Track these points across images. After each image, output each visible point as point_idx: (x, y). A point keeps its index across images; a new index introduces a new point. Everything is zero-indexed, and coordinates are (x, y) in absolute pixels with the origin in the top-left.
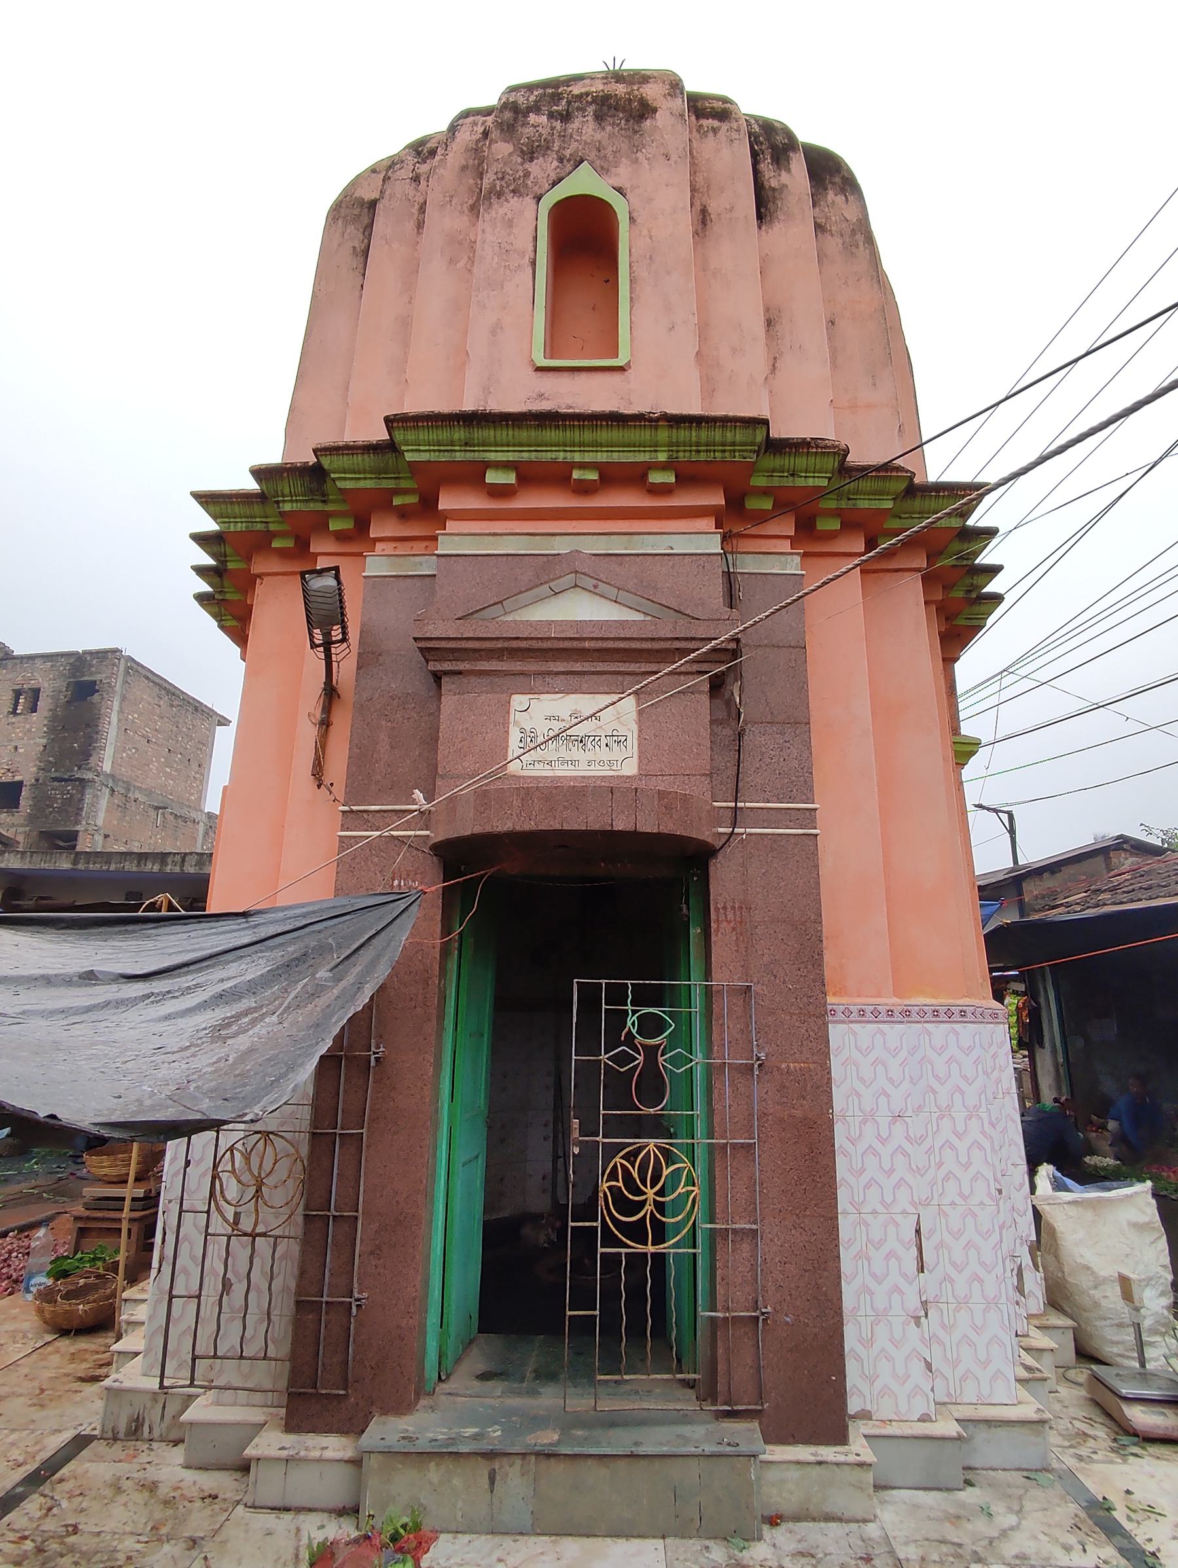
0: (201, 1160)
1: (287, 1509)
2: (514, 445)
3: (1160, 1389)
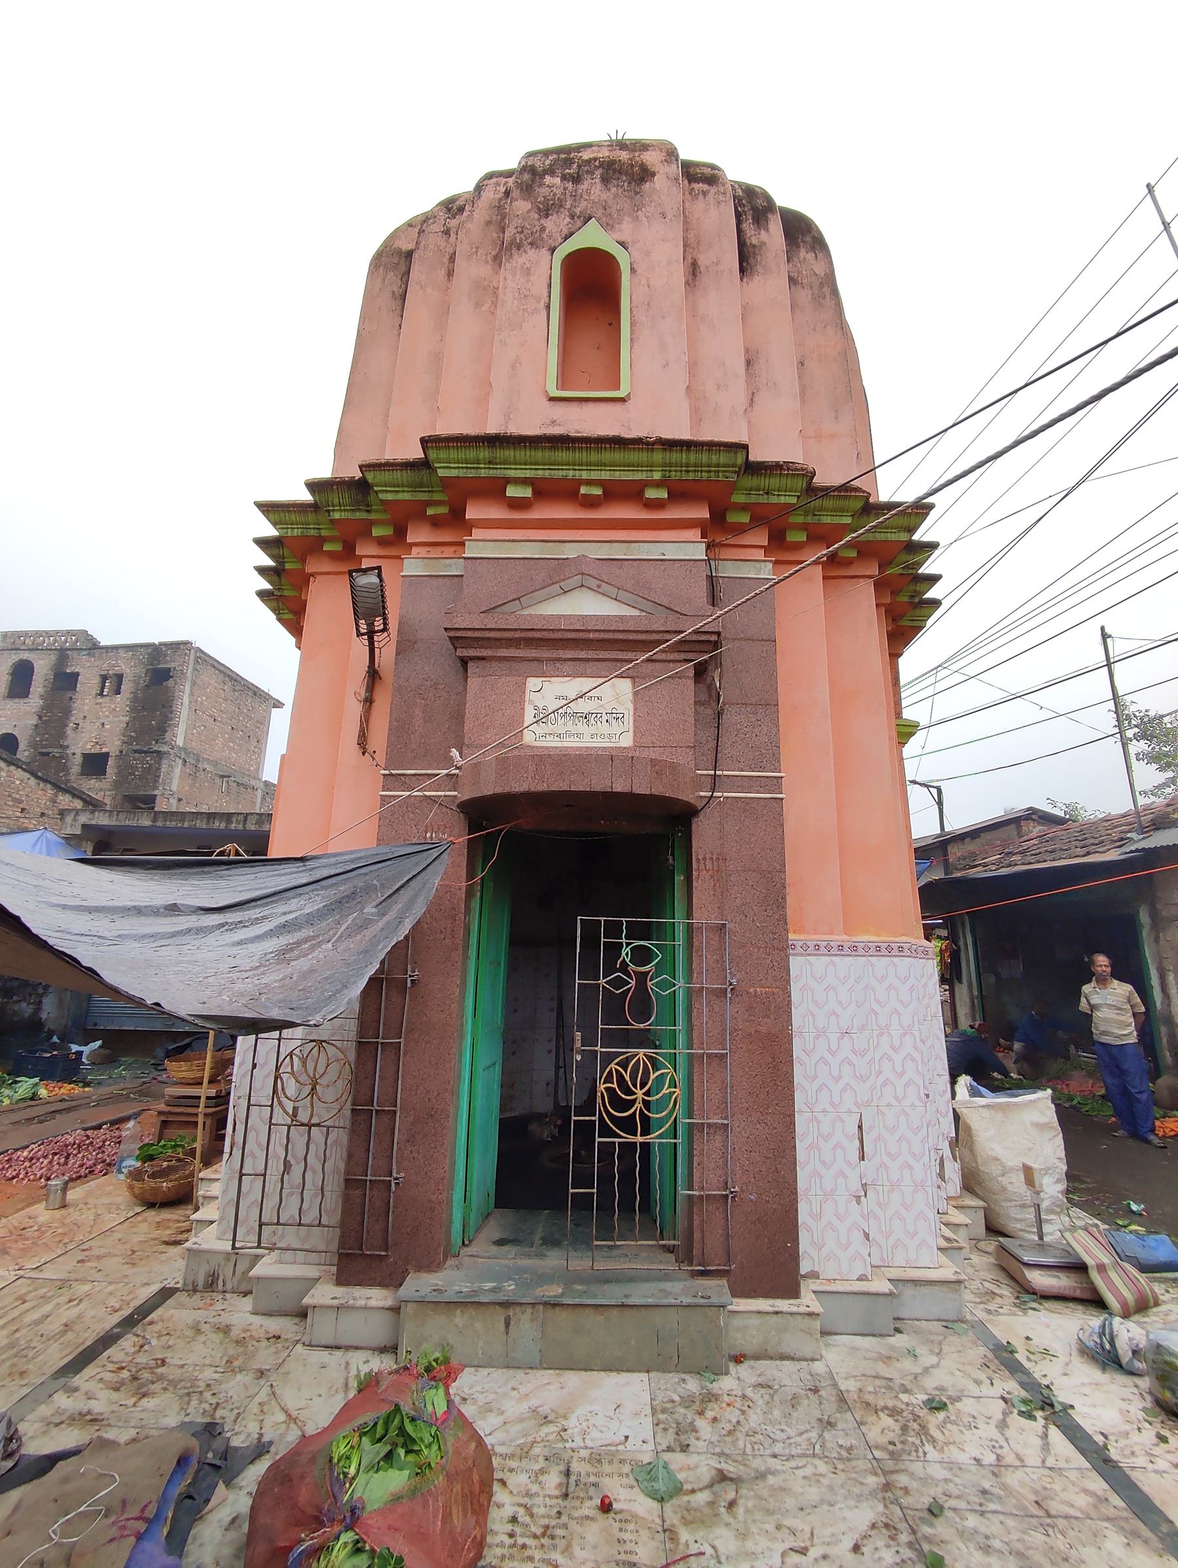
0: (265, 1064)
1: (338, 1348)
2: (531, 464)
3: (1055, 1257)
